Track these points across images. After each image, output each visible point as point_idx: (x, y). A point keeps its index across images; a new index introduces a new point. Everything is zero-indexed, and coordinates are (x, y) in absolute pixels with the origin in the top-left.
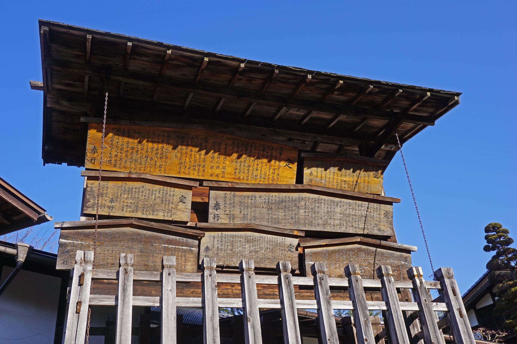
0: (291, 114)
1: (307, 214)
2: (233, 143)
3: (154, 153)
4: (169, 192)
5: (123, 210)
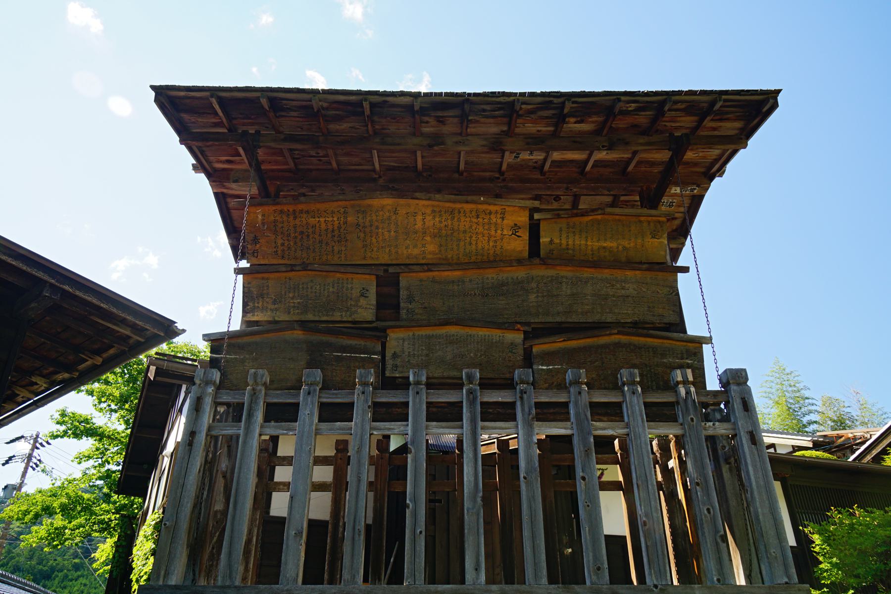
0: (523, 160)
1: (540, 299)
2: (433, 211)
3: (329, 235)
4: (345, 285)
5: (289, 313)
